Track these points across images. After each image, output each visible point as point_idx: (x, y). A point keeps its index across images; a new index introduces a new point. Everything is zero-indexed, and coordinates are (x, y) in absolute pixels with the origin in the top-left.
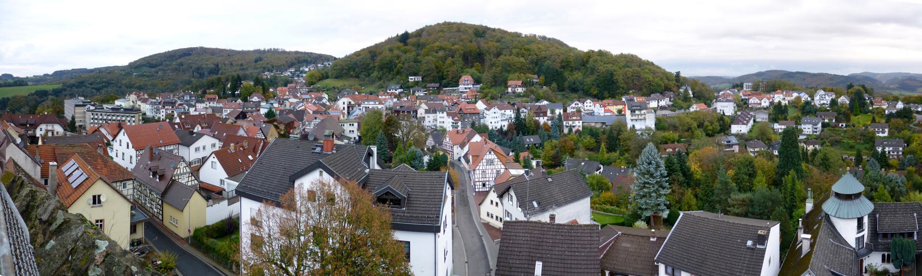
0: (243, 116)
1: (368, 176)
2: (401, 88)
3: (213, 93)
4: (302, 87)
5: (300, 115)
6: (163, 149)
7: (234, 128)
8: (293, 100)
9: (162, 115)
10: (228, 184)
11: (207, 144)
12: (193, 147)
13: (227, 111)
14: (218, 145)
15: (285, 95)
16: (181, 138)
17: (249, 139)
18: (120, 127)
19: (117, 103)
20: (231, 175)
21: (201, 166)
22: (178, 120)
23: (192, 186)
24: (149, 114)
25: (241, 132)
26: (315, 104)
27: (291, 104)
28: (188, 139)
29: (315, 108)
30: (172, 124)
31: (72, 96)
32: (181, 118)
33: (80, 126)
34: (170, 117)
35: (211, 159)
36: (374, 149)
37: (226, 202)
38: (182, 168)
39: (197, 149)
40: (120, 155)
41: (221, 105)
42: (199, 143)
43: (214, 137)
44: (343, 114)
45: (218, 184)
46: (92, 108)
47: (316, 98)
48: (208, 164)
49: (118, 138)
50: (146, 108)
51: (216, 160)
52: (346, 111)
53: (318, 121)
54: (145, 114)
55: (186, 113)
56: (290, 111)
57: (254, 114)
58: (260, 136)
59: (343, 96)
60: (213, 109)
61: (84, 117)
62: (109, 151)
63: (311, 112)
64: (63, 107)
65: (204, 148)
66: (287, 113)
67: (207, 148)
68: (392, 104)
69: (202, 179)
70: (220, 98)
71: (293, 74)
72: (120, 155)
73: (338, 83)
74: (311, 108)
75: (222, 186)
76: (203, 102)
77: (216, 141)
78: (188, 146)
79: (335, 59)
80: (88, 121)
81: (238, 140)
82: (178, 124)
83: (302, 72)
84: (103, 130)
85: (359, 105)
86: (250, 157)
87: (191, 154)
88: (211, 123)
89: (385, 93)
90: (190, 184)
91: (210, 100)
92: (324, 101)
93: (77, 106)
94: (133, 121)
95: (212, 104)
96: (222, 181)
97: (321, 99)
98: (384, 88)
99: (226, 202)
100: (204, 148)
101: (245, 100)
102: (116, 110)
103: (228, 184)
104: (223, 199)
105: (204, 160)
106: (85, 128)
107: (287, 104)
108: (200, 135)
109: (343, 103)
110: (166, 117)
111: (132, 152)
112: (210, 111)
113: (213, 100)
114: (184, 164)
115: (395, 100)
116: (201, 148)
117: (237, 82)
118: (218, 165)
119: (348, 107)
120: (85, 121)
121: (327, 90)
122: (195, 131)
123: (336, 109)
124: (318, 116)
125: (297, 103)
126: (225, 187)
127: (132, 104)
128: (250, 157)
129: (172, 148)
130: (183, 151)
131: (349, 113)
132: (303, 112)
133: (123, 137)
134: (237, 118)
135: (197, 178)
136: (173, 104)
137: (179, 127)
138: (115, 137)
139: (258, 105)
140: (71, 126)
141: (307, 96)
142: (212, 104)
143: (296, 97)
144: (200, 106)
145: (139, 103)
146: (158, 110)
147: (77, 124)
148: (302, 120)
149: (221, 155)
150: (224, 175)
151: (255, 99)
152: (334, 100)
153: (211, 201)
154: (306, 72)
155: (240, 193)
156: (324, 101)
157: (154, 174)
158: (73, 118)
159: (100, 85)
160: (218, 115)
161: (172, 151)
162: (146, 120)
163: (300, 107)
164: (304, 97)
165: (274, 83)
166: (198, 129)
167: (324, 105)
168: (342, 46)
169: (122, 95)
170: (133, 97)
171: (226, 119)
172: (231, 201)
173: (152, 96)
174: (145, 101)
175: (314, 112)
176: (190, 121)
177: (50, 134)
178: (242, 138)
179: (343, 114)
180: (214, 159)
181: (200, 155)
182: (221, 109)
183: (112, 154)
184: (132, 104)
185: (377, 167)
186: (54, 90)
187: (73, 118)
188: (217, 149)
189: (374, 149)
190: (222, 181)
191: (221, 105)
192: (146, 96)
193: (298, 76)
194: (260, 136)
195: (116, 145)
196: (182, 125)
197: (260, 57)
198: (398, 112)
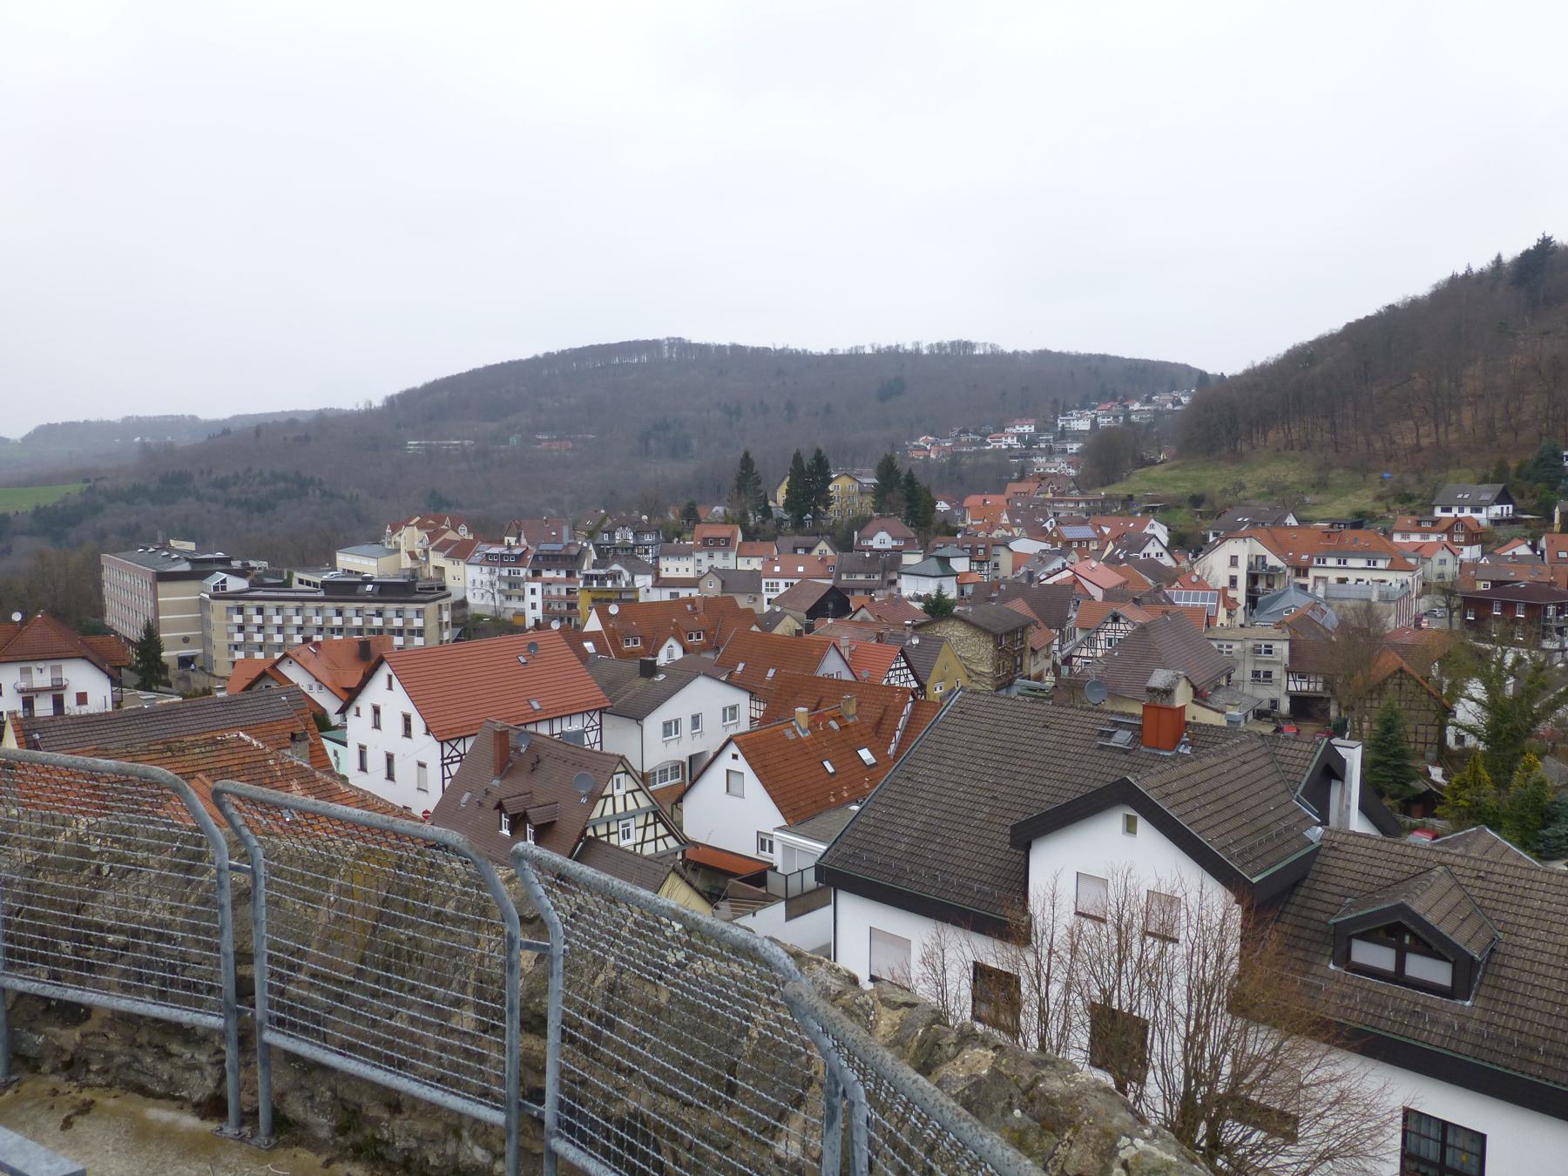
0: (835, 603)
1: (1316, 851)
2: (1503, 498)
3: (727, 521)
4: (1061, 495)
5: (1055, 606)
6: (544, 729)
7: (804, 650)
8: (1027, 546)
9: (532, 605)
10: (788, 849)
11: (709, 708)
12: (654, 722)
13: (778, 581)
14: (748, 709)
15: (993, 526)
16: (610, 687)
17: (859, 687)
18: (369, 658)
19: (350, 561)
20: (797, 808)
21: (686, 791)
22: (593, 624)
23: (658, 858)
24: (479, 602)
25: (833, 666)
26: (1112, 561)
27: (1019, 558)
28: (635, 690)
29: (1112, 578)
30: (574, 635)
31: (130, 539)
32: (604, 617)
33: (185, 662)
34: (565, 613)
35: (725, 762)
36: (1353, 756)
37: (780, 909)
38: (621, 795)
39: (669, 728)
40: (376, 762)
41: (756, 564)
42: (678, 707)
43: (731, 682)
44: (1231, 605)
45: (749, 849)
46: (236, 584)
47: (1117, 539)
48: (714, 779)
49: (365, 702)
50: (471, 582)
51: (742, 765)
52: (1240, 594)
53: (1123, 630)
54: (463, 603)
55: (627, 598)
56: (1017, 589)
57: (879, 596)
58: (902, 679)
59: (1232, 532)
60: (728, 579)
61: (204, 623)
62: (330, 746)
63: (1098, 594)
64: (99, 585)
65: (696, 721)
66: (1005, 597)
67: (705, 722)
68: (1451, 568)
69: (691, 830)
70: (749, 536)
71: (1029, 442)
72: (376, 762)
73: (1214, 479)
74: (1097, 578)
75: (765, 856)
76: (687, 553)
77: (741, 699)
78: (637, 715)
79: (1203, 377)
80: (219, 641)
81: (823, 694)
82: (592, 636)
83: (1064, 435)
84: (293, 673)
85: (1302, 571)
86: (866, 755)
87: (652, 745)
88: (719, 636)
89: (1423, 520)
90: (649, 849)
91: (712, 544)
92: (1152, 549)
93: (163, 577)
94: (424, 623)
95: (719, 561)
96: (764, 842)
97: (1142, 541)
98: (1416, 503)
99: (780, 909)
100: (696, 721)
101: (843, 544)
102: (346, 590)
103: (788, 849)
104: (769, 899)
105: (695, 768)
106: (206, 669)
107: (1005, 560)
108: (680, 678)
109: (1226, 562)
110: (549, 613)
111: (426, 748)
112: (712, 588)
113: (724, 544)
114: (627, 783)
115: (1470, 553)
116: (686, 724)
117: (810, 483)
118: (752, 784)
119: (1253, 578)
120: (206, 641)
121: (1161, 509)
122: (662, 659)
123: (1201, 584)
124: (1125, 610)
125: (1043, 558)
126: (777, 858)
127: (407, 563)
128: (866, 755)
129: (576, 725)
130: (618, 738)
131: (1252, 600)
132: (1070, 593)
133: (387, 696)
134: (816, 612)
135: (675, 830)
136: (570, 562)
137: (600, 648)
138: (350, 696)
139: (889, 564)
140: (141, 663)
141: (1085, 532)
142: (719, 561)
143: (1038, 533)
144: (673, 568)
145: (437, 559)
146: (515, 584)
147: (168, 655)
148: (1060, 623)
149: (764, 753)
150: (769, 816)
151: (882, 540)
152: (1188, 543)
153: (725, 906)
154: (1077, 436)
155: (835, 878)
156: (1152, 549)
157: (518, 823)
158: (151, 632)
159: (271, 495)
160: (743, 602)
161: (579, 735)
162: (469, 626)
163: (1056, 575)
164: (1070, 532)
165: (965, 477)
166: (670, 653)
167: (1152, 567)
168: (1233, 330)
169: (369, 534)
170: (411, 538)
171: (774, 618)
172: (799, 905)
173: (488, 530)
174: (460, 552)
175: (1109, 594)
176: (635, 631)
177: (43, 707)
178: (840, 686)
179: (1231, 605)
180: (734, 761)
181: (681, 750)
182: (755, 576)
183: (345, 761)
184: (407, 563)
185: (1358, 823)
186: (38, 513)
187: (151, 632)
188: (744, 726)
189: (1353, 756)
190: (764, 842)
191: (756, 564)
192: (464, 533)
193: (1049, 452)
194: (902, 679)
195: (358, 727)
196: (612, 637)
197: (892, 380)
198: (1478, 604)
